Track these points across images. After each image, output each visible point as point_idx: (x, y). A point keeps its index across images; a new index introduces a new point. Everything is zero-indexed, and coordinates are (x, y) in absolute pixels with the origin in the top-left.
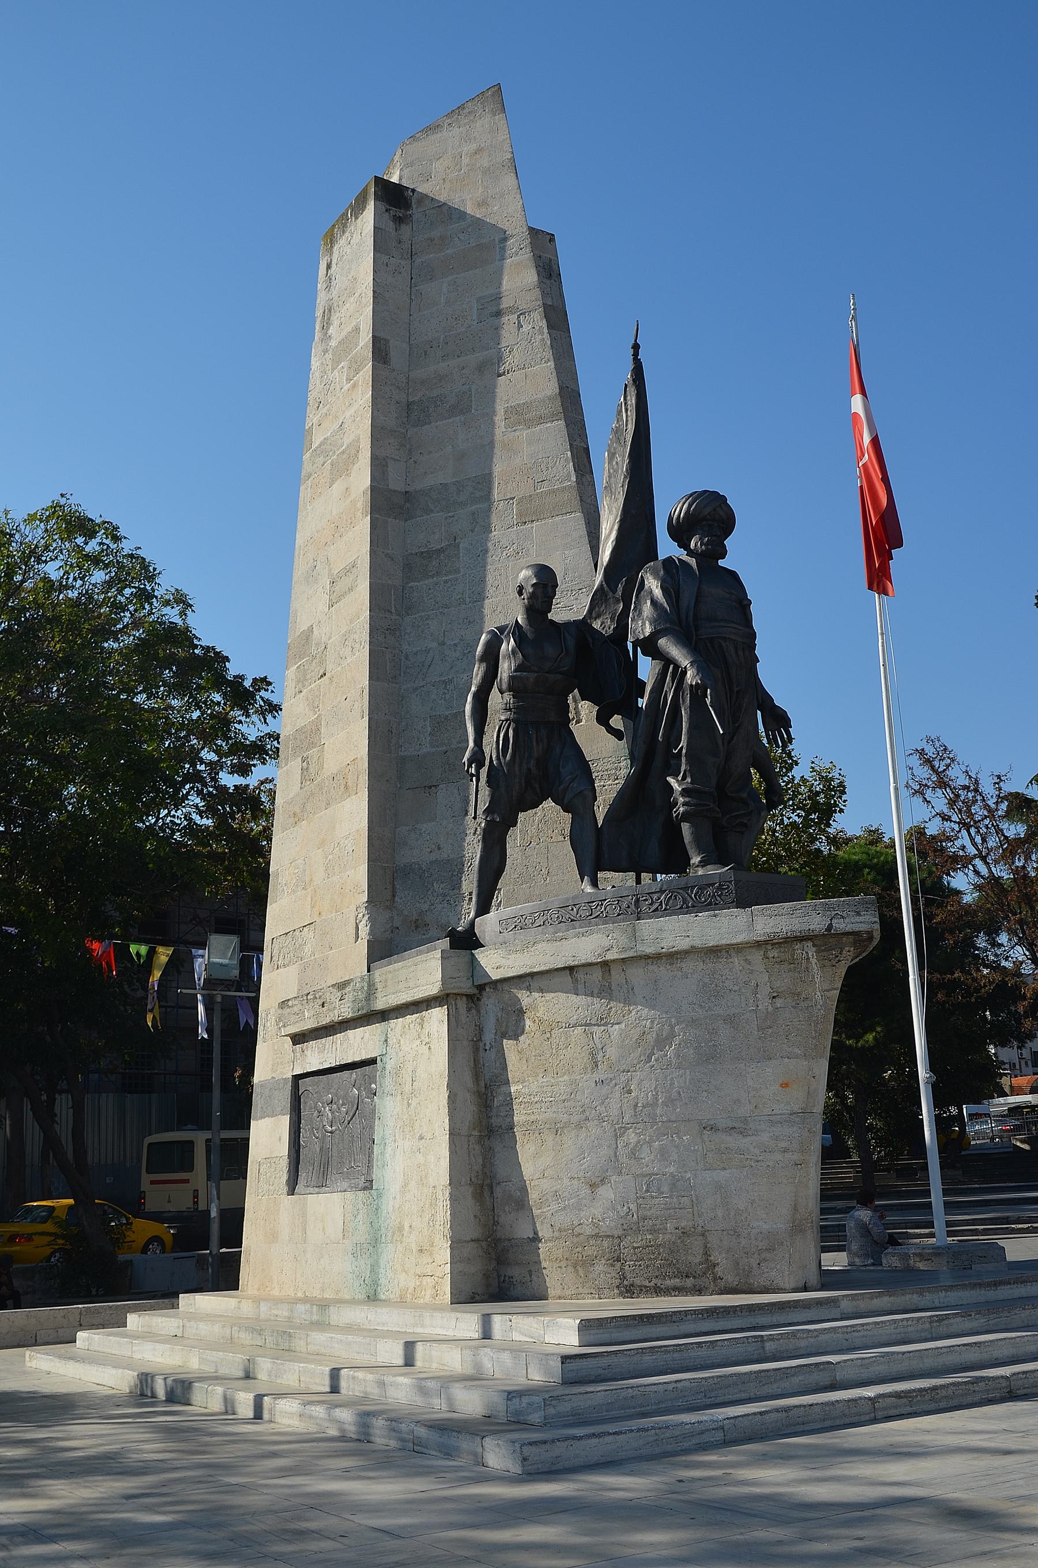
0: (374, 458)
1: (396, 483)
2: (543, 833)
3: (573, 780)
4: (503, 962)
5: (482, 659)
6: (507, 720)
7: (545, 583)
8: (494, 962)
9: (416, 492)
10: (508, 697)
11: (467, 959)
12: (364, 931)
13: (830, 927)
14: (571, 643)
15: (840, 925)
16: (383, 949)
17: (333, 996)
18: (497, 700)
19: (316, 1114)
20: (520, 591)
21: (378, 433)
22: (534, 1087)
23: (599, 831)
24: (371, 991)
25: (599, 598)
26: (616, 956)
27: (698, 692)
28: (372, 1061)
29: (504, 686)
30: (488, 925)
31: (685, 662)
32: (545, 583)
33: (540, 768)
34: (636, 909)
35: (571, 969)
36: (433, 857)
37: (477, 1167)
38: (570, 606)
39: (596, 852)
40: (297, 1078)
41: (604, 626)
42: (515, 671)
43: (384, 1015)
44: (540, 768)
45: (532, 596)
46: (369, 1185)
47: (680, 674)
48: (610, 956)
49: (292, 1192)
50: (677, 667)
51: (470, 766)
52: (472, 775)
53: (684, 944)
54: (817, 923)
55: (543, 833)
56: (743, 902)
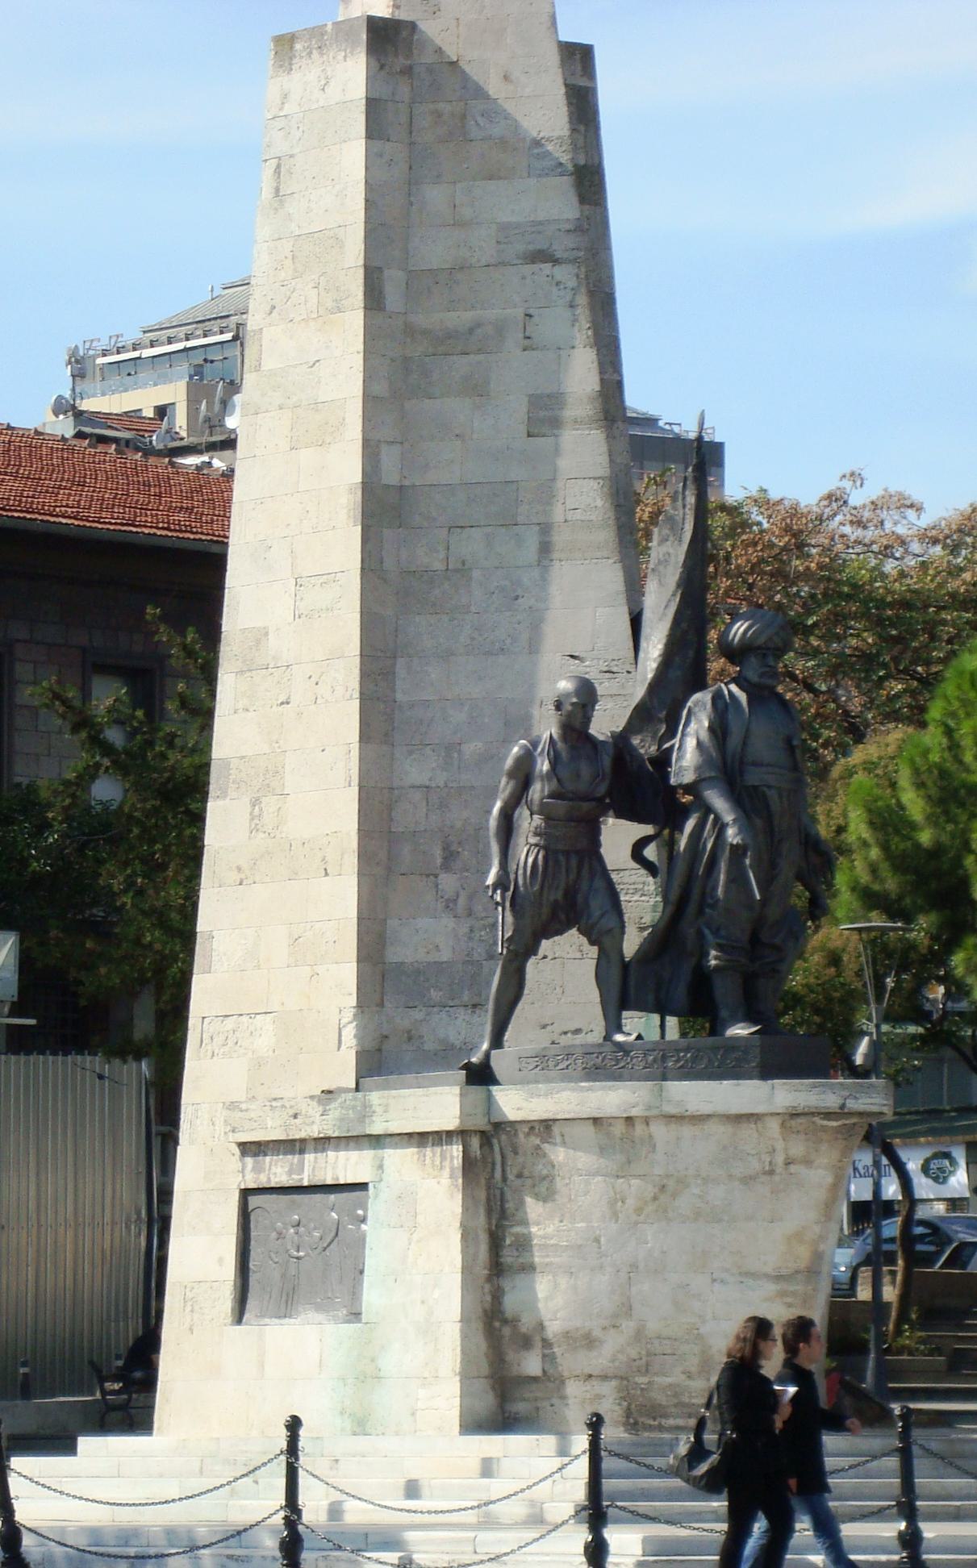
0: (367, 443)
1: (391, 475)
2: (566, 969)
3: (602, 915)
4: (524, 1104)
5: (511, 774)
6: (536, 845)
7: (587, 695)
8: (514, 1102)
9: (414, 486)
10: (538, 820)
11: (484, 1095)
12: (350, 1034)
13: (843, 1106)
14: (607, 762)
15: (852, 1105)
16: (376, 1063)
17: (314, 1110)
18: (528, 823)
19: (274, 1235)
20: (558, 706)
21: (371, 402)
22: (550, 1229)
23: (625, 967)
24: (365, 1113)
25: (642, 716)
26: (641, 1114)
27: (738, 851)
28: (363, 1186)
29: (535, 808)
30: (500, 1063)
31: (728, 818)
32: (587, 695)
33: (567, 896)
34: (662, 1064)
35: (596, 1121)
36: (430, 958)
37: (488, 1306)
38: (606, 723)
39: (624, 988)
40: (246, 1193)
41: (645, 746)
42: (550, 796)
43: (376, 1141)
44: (567, 896)
45: (570, 715)
46: (355, 1316)
47: (720, 828)
48: (634, 1112)
49: (239, 1315)
50: (717, 819)
51: (494, 891)
52: (497, 904)
53: (706, 1109)
54: (831, 1101)
55: (566, 969)
56: (769, 1071)
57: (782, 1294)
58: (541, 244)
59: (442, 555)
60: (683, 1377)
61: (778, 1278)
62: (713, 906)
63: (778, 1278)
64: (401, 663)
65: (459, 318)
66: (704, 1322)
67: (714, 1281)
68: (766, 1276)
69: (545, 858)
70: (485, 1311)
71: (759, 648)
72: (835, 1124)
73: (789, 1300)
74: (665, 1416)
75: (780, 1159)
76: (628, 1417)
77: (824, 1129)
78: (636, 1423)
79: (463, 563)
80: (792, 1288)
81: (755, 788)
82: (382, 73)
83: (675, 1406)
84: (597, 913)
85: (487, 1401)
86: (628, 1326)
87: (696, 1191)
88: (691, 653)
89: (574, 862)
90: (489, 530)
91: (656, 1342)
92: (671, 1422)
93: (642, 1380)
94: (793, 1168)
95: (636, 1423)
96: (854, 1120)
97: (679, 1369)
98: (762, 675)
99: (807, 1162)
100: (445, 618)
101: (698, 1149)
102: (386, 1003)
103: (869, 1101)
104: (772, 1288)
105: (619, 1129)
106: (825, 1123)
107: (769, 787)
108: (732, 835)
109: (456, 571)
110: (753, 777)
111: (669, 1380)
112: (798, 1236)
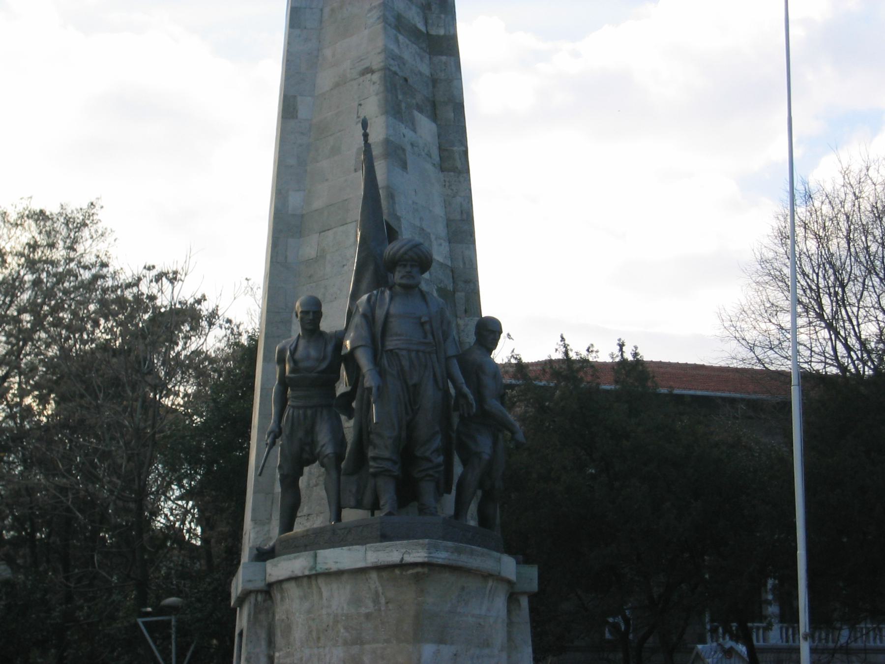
15: (409, 559)
81: (391, 350)
103: (419, 555)
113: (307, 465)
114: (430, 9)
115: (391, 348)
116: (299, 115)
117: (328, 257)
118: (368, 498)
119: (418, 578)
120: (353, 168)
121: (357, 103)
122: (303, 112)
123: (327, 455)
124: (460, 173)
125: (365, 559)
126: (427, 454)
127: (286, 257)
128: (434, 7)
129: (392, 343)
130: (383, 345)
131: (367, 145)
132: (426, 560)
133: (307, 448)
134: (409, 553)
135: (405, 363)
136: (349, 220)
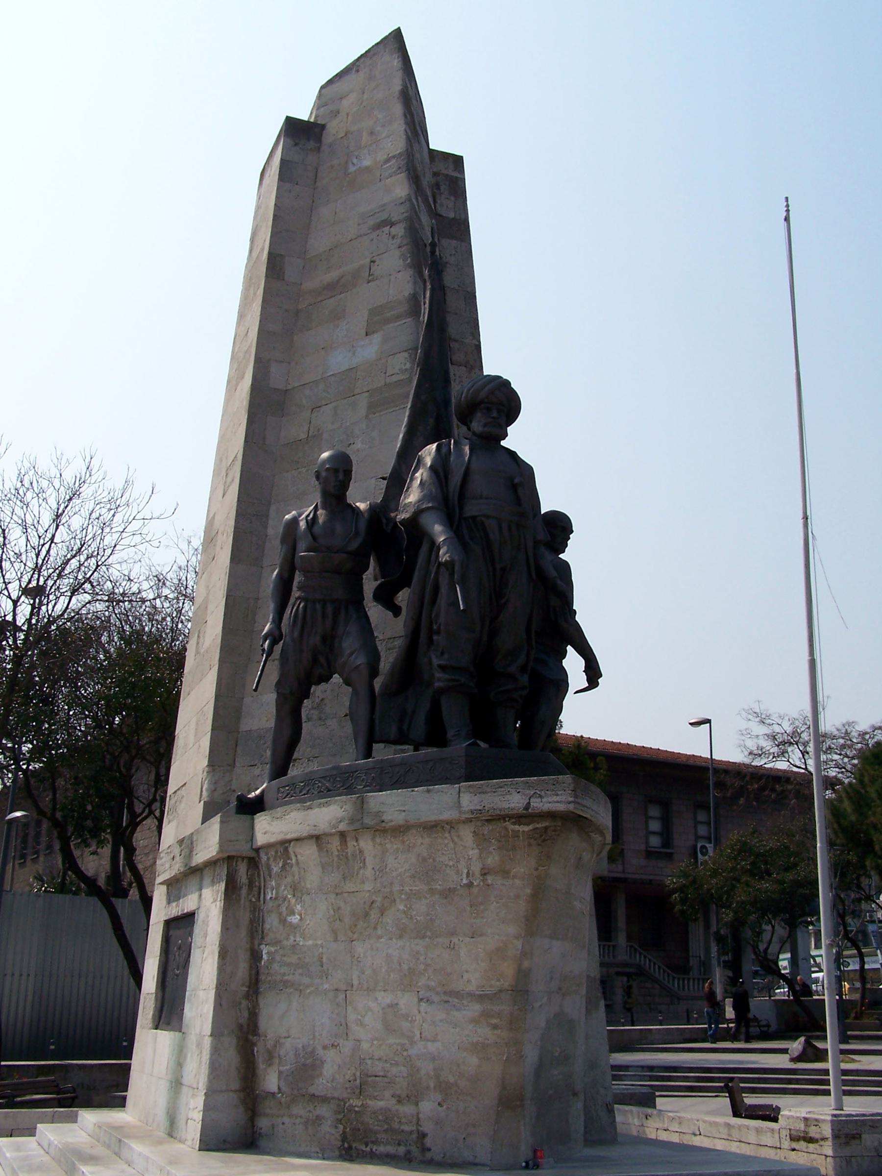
13: (527, 807)
14: (362, 525)
15: (539, 805)
20: (318, 477)
37: (243, 1021)
57: (486, 1014)
58: (384, 216)
59: (306, 429)
60: (393, 1101)
61: (482, 998)
62: (438, 632)
63: (482, 998)
64: (273, 508)
65: (334, 275)
66: (413, 1043)
67: (421, 1000)
68: (471, 995)
69: (305, 607)
70: (241, 1027)
71: (482, 402)
72: (526, 828)
73: (495, 1021)
74: (376, 1142)
75: (476, 868)
76: (343, 1141)
77: (516, 834)
78: (350, 1148)
79: (319, 430)
80: (497, 1008)
81: (474, 518)
82: (297, 148)
83: (386, 1131)
84: (347, 652)
85: (231, 1117)
86: (347, 1047)
87: (402, 907)
88: (431, 421)
89: (330, 609)
90: (333, 404)
91: (369, 1062)
92: (382, 1149)
93: (356, 1102)
94: (490, 879)
95: (350, 1148)
96: (545, 824)
97: (387, 1094)
98: (485, 425)
99: (505, 873)
100: (304, 470)
101: (400, 860)
102: (237, 764)
103: (555, 798)
104: (476, 1008)
105: (335, 843)
106: (517, 827)
107: (488, 517)
108: (444, 555)
109: (314, 436)
110: (472, 509)
111: (381, 1104)
112: (500, 952)
113: (318, 683)
114: (439, 189)
115: (475, 513)
116: (286, 278)
117: (326, 436)
118: (419, 728)
119: (543, 838)
120: (363, 332)
121: (368, 260)
122: (291, 272)
123: (357, 667)
124: (472, 368)
125: (459, 804)
126: (513, 669)
127: (264, 438)
128: (442, 188)
129: (472, 509)
130: (461, 508)
131: (67, 608)
132: (571, 807)
133: (322, 660)
134: (541, 796)
135: (494, 536)
136: (357, 391)
